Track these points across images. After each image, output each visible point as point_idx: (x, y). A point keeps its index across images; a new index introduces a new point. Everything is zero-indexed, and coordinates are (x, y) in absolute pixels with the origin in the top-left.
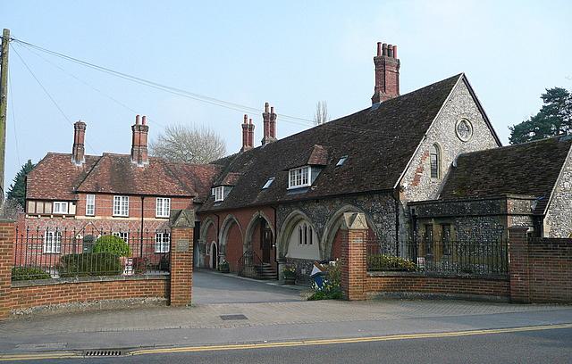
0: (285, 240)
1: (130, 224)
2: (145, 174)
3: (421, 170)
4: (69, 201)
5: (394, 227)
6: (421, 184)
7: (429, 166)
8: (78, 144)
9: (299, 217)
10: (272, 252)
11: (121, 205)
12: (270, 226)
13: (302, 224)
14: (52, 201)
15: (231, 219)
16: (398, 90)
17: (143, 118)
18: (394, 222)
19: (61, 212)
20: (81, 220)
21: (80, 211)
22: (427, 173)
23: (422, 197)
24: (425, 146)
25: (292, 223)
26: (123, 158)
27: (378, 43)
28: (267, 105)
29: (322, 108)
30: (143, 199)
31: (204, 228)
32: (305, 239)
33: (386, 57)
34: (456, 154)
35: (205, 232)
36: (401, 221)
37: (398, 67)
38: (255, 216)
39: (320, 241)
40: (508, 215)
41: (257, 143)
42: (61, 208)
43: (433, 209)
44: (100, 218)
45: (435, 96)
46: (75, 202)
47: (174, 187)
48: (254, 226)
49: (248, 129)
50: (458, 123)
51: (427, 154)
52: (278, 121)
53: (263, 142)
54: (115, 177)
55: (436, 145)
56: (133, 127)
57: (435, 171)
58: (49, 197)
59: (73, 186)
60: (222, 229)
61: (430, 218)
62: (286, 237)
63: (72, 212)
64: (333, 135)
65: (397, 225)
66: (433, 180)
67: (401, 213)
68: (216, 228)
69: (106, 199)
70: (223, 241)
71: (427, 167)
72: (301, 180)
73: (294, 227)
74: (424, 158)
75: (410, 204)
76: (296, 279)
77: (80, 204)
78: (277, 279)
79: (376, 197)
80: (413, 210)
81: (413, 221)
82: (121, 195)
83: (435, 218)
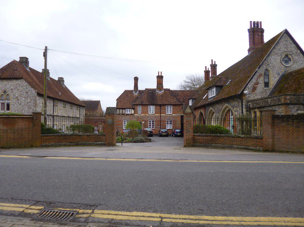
1: (156, 117)
4: (131, 109)
11: (152, 109)
17: (161, 72)
19: (128, 113)
20: (136, 116)
27: (251, 22)
28: (212, 61)
30: (160, 106)
34: (281, 74)
38: (200, 111)
43: (257, 104)
44: (175, 115)
46: (134, 109)
47: (174, 101)
57: (267, 84)
59: (133, 102)
61: (255, 108)
63: (133, 112)
67: (244, 106)
75: (248, 102)
80: (250, 104)
82: (170, 105)
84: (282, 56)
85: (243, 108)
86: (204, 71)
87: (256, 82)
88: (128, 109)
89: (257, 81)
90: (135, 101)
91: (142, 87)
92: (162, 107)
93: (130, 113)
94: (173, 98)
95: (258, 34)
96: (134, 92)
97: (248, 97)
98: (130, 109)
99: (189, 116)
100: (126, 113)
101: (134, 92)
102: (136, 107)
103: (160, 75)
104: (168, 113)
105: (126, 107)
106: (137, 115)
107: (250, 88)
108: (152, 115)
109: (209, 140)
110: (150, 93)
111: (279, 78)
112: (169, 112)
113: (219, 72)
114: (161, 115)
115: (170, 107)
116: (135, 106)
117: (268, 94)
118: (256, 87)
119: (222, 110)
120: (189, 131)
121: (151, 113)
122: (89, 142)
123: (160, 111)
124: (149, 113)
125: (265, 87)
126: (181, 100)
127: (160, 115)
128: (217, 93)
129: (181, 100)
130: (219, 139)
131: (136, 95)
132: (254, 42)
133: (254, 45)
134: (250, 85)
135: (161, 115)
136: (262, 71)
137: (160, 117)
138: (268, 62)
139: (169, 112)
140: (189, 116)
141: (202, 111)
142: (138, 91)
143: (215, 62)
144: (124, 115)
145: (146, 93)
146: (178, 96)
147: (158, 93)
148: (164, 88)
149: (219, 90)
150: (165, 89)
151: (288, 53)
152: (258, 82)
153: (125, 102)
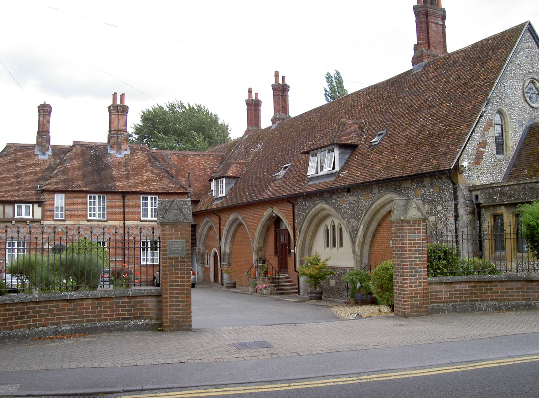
0: (307, 242)
2: (127, 165)
3: (483, 144)
4: (33, 203)
5: (452, 220)
6: (486, 162)
7: (493, 140)
8: (43, 132)
9: (324, 213)
10: (290, 260)
11: (96, 209)
12: (287, 224)
13: (328, 223)
14: (12, 203)
15: (237, 219)
16: (445, 46)
18: (452, 213)
19: (24, 217)
20: (49, 226)
21: (47, 214)
22: (491, 148)
23: (485, 179)
24: (489, 113)
25: (315, 221)
26: (102, 144)
29: (335, 83)
30: (124, 198)
31: (202, 231)
32: (333, 240)
33: (429, 5)
34: (526, 124)
35: (203, 237)
36: (462, 211)
37: (444, 18)
39: (353, 243)
40: (124, 221)
41: (266, 120)
42: (24, 212)
43: (503, 194)
45: (494, 51)
46: (40, 204)
48: (266, 229)
49: (253, 106)
50: (527, 84)
51: (490, 124)
52: (291, 94)
53: (274, 121)
54: (88, 171)
55: (500, 112)
56: (109, 108)
57: (500, 146)
58: (9, 198)
60: (224, 233)
62: (308, 238)
64: (348, 116)
65: (456, 217)
66: (500, 157)
67: (461, 200)
68: (216, 230)
69: (78, 199)
70: (226, 248)
71: (491, 142)
72: (324, 165)
73: (318, 226)
74: (486, 130)
75: (472, 189)
76: (323, 288)
77: (47, 205)
78: (298, 293)
79: (427, 181)
80: (477, 197)
81: (477, 211)
83: (505, 205)
84: (525, 82)
85: (459, 206)
86: (246, 101)
87: (481, 140)
88: (23, 205)
89: (484, 139)
90: (42, 178)
91: (61, 136)
92: (129, 199)
93: (31, 217)
94: (158, 175)
95: (436, 21)
96: (37, 152)
97: (468, 176)
98: (31, 205)
99: (417, 229)
100: (16, 217)
101: (37, 152)
102: (45, 197)
103: (118, 102)
104: (147, 216)
105: (17, 199)
106: (51, 222)
107: (471, 155)
108: (100, 223)
109: (466, 294)
110: (91, 157)
111: (521, 133)
112: (97, 215)
113: (296, 109)
114: (127, 223)
115: (152, 200)
116: (46, 194)
117: (505, 170)
118: (481, 151)
119: (371, 210)
120: (417, 272)
121: (94, 216)
122: (99, 321)
123: (123, 210)
124: (89, 218)
125: (498, 153)
126: (183, 181)
127: (122, 223)
128: (342, 164)
129: (183, 181)
130: (492, 289)
131: (43, 160)
132: (428, 40)
133: (429, 46)
134: (470, 149)
135: (127, 223)
136: (492, 115)
137: (122, 231)
138: (500, 93)
139: (97, 215)
140: (417, 229)
141: (282, 212)
142: (50, 149)
143: (283, 78)
144: (11, 222)
145: (75, 154)
146: (171, 169)
147: (112, 156)
148: (53, 142)
149: (347, 156)
150: (55, 148)
151: (535, 77)
152: (486, 141)
153: (12, 180)
